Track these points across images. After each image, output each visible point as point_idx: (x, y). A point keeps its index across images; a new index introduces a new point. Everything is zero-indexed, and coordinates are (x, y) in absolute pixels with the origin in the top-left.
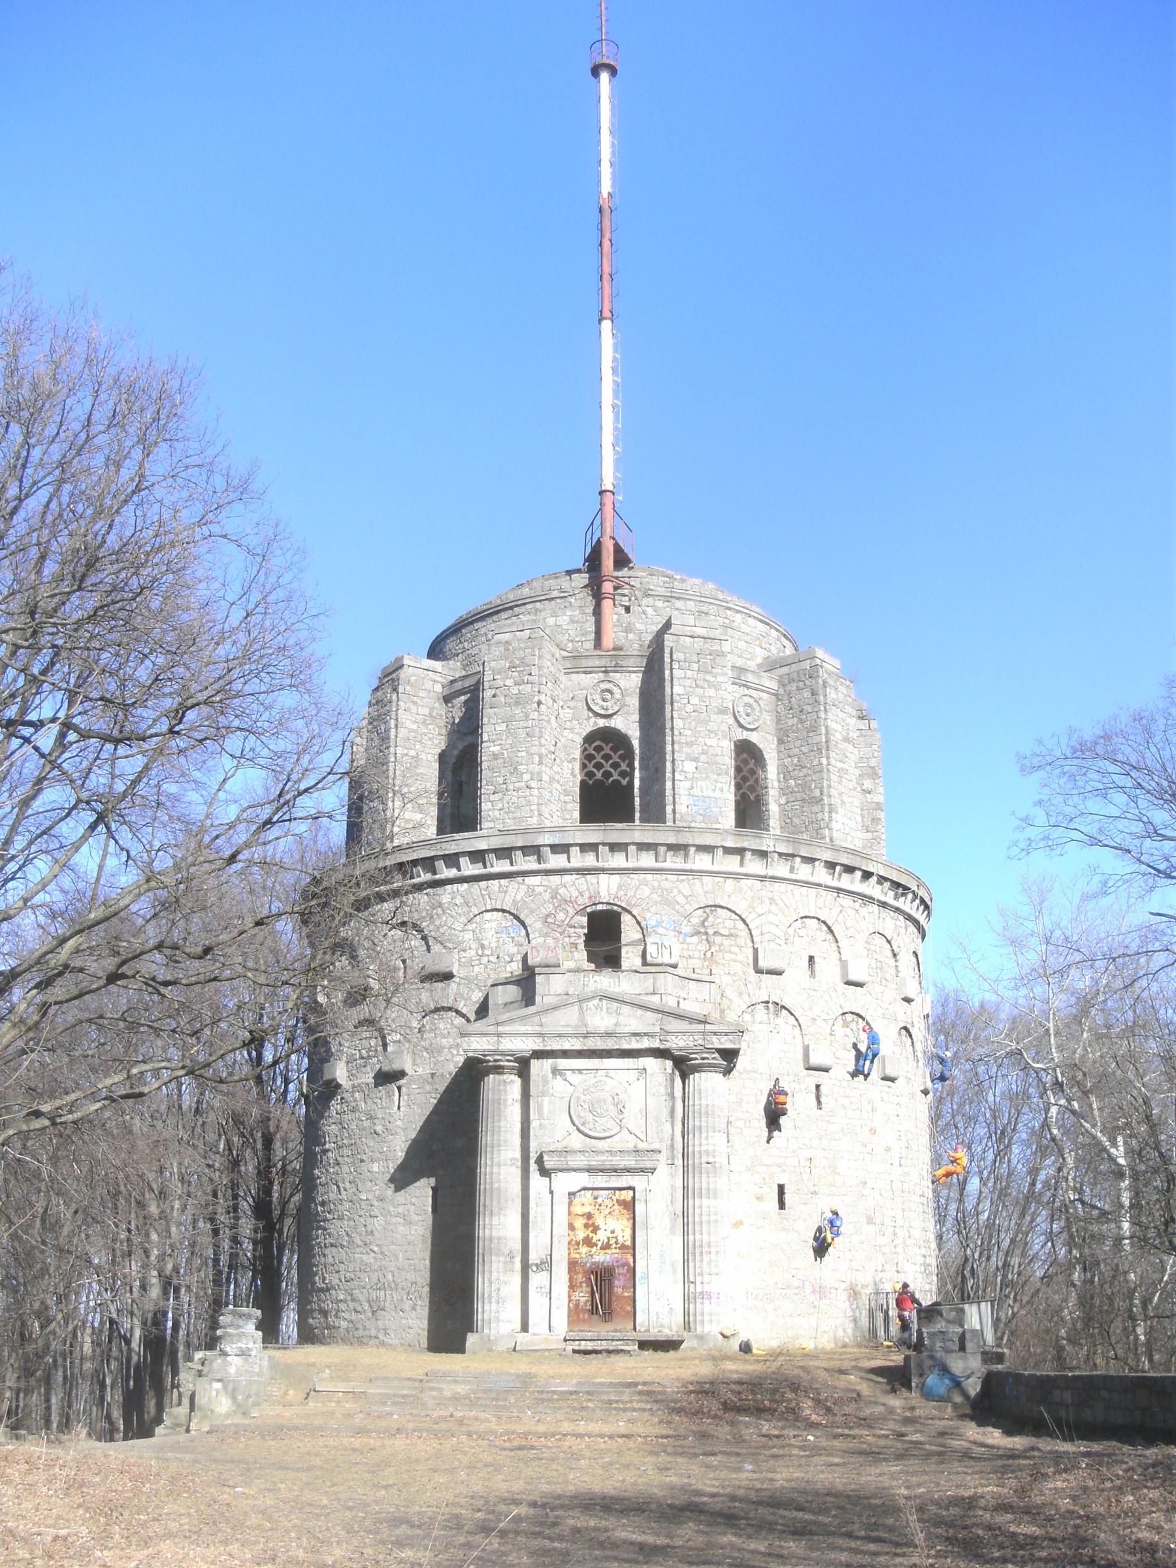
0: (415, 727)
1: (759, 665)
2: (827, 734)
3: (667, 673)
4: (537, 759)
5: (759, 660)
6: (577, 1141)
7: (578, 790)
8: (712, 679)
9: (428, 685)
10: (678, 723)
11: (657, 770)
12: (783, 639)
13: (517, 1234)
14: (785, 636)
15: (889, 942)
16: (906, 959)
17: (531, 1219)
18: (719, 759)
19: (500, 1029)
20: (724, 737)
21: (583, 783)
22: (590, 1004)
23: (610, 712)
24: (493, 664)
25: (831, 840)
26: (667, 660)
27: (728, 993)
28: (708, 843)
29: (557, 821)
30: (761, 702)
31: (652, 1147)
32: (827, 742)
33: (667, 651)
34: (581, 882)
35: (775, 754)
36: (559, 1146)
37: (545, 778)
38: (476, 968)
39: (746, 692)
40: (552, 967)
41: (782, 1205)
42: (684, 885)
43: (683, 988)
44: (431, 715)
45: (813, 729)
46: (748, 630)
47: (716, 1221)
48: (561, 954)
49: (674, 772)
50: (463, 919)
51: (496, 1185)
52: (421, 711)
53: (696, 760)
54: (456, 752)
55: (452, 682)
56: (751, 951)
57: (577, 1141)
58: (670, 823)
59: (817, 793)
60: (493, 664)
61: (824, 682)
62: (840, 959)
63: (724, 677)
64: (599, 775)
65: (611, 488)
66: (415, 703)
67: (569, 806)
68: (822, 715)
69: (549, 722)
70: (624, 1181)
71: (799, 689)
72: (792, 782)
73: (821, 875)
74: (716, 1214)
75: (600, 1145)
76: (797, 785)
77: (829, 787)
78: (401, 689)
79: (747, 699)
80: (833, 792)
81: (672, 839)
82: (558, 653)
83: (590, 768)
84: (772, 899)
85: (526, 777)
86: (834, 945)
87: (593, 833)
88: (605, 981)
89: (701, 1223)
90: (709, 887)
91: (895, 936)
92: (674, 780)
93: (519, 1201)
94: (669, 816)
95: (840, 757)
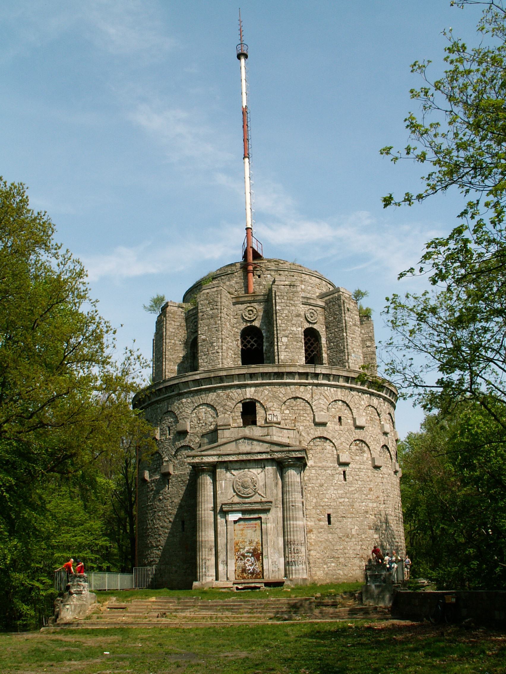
0: (174, 331)
1: (317, 297)
2: (345, 323)
3: (274, 301)
4: (220, 340)
5: (318, 294)
6: (236, 499)
7: (240, 352)
8: (293, 303)
9: (179, 313)
10: (279, 322)
11: (272, 343)
12: (329, 285)
13: (213, 539)
14: (329, 284)
15: (376, 409)
16: (385, 416)
17: (218, 532)
18: (297, 336)
19: (203, 453)
20: (299, 326)
21: (242, 349)
22: (240, 441)
23: (252, 319)
24: (202, 302)
25: (349, 367)
26: (274, 295)
27: (303, 434)
28: (291, 371)
29: (231, 364)
30: (318, 312)
31: (268, 500)
32: (346, 326)
33: (274, 292)
34: (239, 391)
35: (325, 333)
36: (230, 501)
37: (224, 348)
38: (197, 429)
39: (311, 307)
40: (227, 426)
41: (329, 522)
42: (283, 389)
43: (281, 432)
44: (180, 325)
45: (340, 321)
46: (312, 282)
47: (297, 530)
48: (231, 421)
49: (277, 342)
50: (192, 409)
51: (203, 519)
52: (176, 324)
53: (287, 337)
54: (191, 340)
55: (189, 311)
56: (312, 415)
57: (236, 499)
58: (277, 364)
59: (342, 348)
60: (202, 302)
61: (344, 301)
62: (353, 418)
63: (298, 301)
64: (249, 346)
65: (250, 227)
66: (174, 321)
67: (236, 359)
68: (343, 315)
69: (226, 325)
70: (256, 516)
71: (333, 305)
72: (332, 344)
73: (342, 383)
74: (297, 527)
75: (247, 500)
76: (334, 345)
77: (347, 345)
78: (167, 315)
79: (311, 311)
80: (349, 347)
81: (276, 370)
82: (229, 295)
83: (245, 343)
84: (321, 393)
85: (216, 348)
86: (350, 412)
87: (310, 369)
88: (248, 431)
89: (290, 531)
90: (293, 390)
91: (379, 406)
92: (278, 345)
93: (213, 525)
94: (277, 361)
95: (352, 332)
